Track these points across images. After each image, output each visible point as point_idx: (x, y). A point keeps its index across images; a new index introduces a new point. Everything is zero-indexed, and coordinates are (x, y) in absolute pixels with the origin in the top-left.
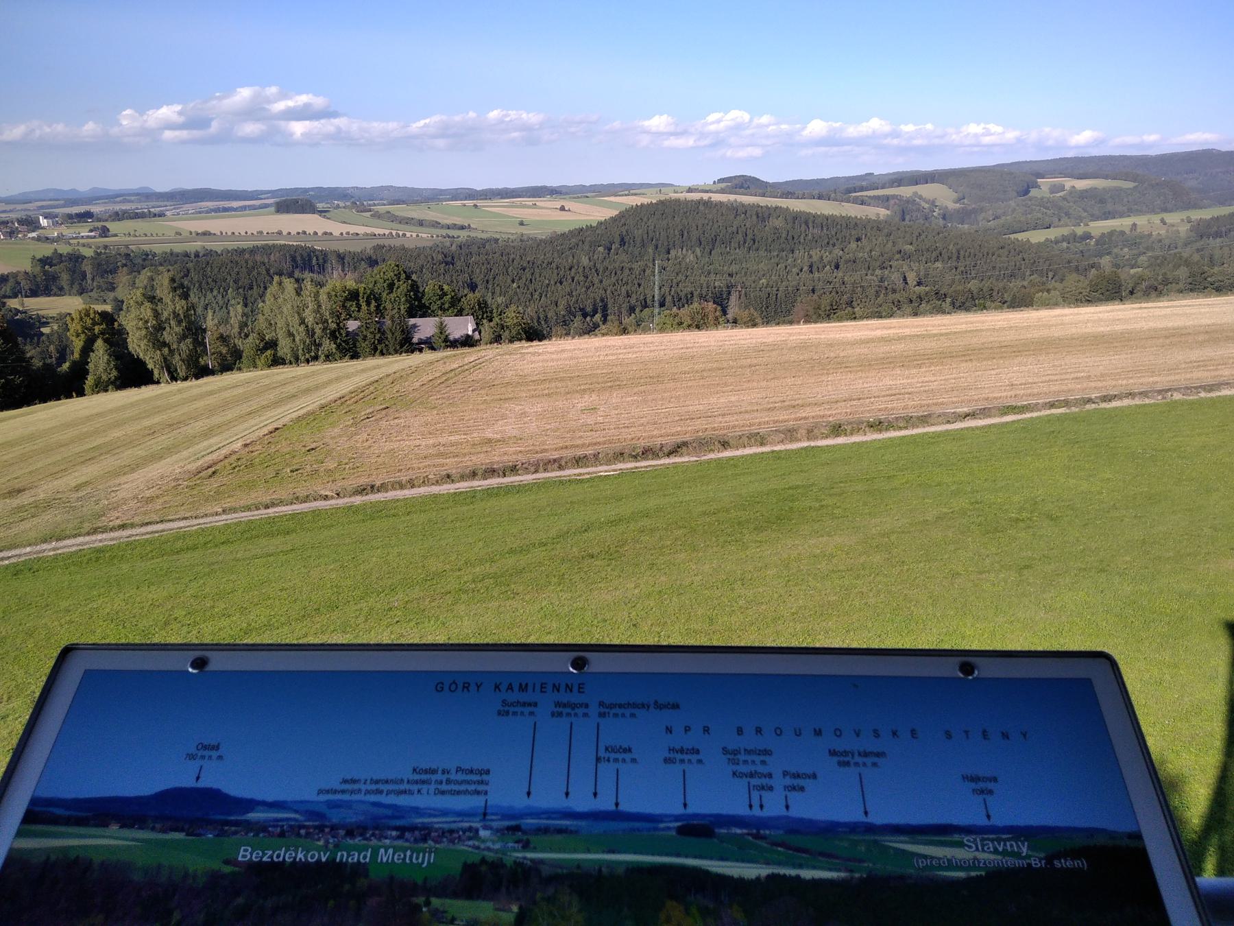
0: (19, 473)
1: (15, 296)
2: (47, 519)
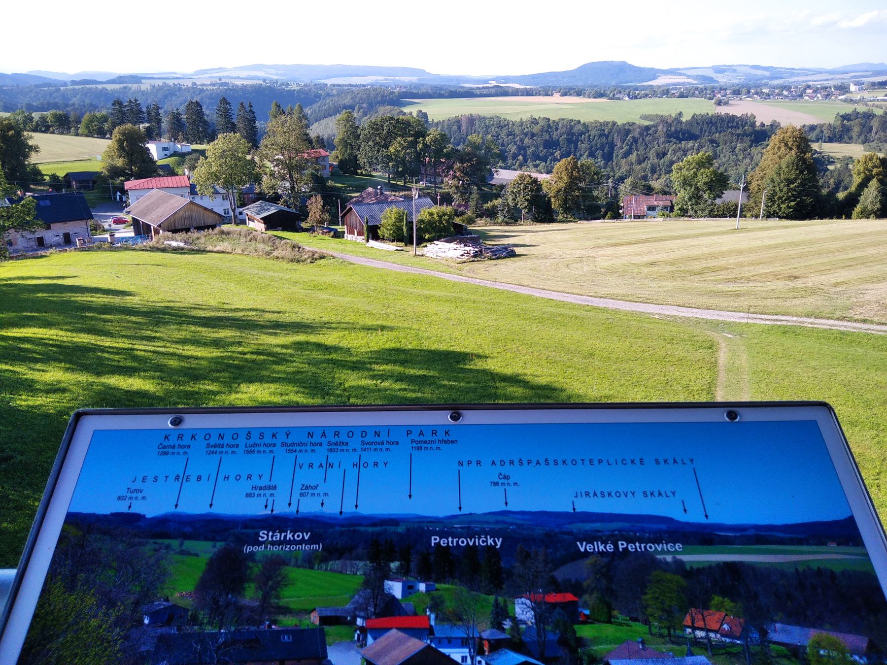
0: (798, 265)
1: (817, 141)
2: (811, 302)
